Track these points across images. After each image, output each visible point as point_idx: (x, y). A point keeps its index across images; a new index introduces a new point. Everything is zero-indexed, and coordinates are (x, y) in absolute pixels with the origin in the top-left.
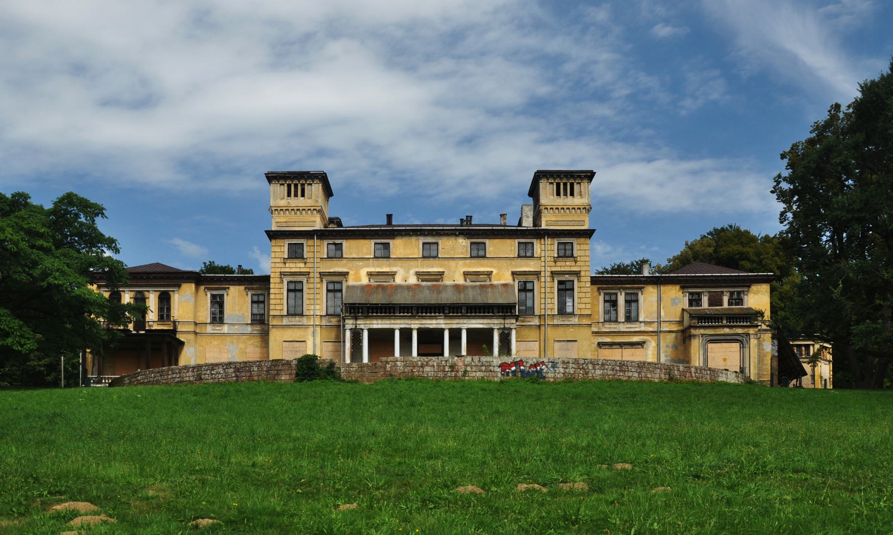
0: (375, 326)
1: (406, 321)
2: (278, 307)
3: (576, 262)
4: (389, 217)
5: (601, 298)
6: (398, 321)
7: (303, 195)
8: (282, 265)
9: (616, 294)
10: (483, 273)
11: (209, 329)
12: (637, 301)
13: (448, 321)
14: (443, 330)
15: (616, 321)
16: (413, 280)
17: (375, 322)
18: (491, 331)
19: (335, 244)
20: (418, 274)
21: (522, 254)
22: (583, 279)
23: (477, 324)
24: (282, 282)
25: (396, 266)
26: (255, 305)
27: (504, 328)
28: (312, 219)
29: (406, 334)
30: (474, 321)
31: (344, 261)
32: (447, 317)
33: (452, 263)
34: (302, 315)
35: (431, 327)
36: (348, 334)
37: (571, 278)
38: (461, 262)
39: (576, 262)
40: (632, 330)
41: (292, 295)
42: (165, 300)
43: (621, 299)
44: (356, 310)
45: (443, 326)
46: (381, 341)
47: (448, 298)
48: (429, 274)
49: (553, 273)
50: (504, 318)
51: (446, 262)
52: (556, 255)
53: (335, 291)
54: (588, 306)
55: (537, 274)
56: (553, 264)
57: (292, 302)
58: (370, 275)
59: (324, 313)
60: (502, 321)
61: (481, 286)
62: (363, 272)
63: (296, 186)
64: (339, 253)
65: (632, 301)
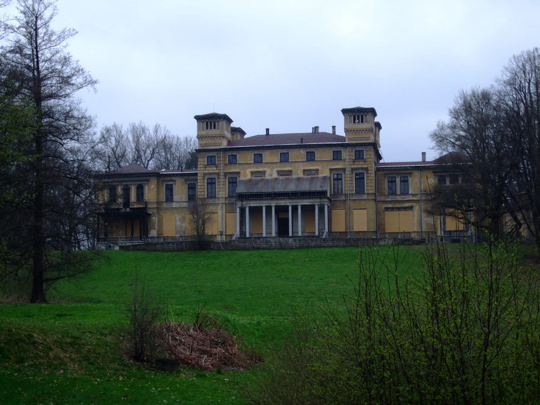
0: (252, 205)
1: (269, 202)
2: (202, 193)
3: (365, 162)
4: (267, 130)
5: (386, 180)
6: (265, 202)
7: (215, 128)
8: (203, 169)
9: (395, 177)
10: (313, 170)
11: (165, 205)
12: (407, 181)
13: (290, 201)
14: (288, 206)
15: (395, 194)
16: (275, 175)
17: (252, 202)
18: (314, 206)
19: (233, 155)
20: (279, 172)
21: (336, 158)
22: (369, 172)
23: (307, 202)
24: (204, 179)
25: (266, 167)
26: (191, 190)
27: (321, 204)
28: (220, 141)
29: (269, 208)
30: (304, 201)
31: (238, 166)
32: (290, 199)
33: (297, 164)
34: (215, 197)
35: (282, 204)
36: (238, 210)
37: (363, 172)
38: (301, 164)
39: (365, 162)
40: (405, 199)
41: (209, 186)
42: (140, 189)
43: (398, 180)
44: (242, 197)
45: (288, 204)
46: (256, 212)
47: (292, 188)
48: (284, 171)
49: (353, 169)
50: (321, 198)
51: (293, 164)
52: (354, 158)
53: (233, 183)
54: (372, 188)
55: (344, 170)
56: (352, 163)
57: (210, 190)
58: (252, 173)
59: (227, 196)
60: (319, 200)
61: (312, 178)
62: (248, 172)
63: (211, 123)
64: (235, 160)
65: (405, 181)
